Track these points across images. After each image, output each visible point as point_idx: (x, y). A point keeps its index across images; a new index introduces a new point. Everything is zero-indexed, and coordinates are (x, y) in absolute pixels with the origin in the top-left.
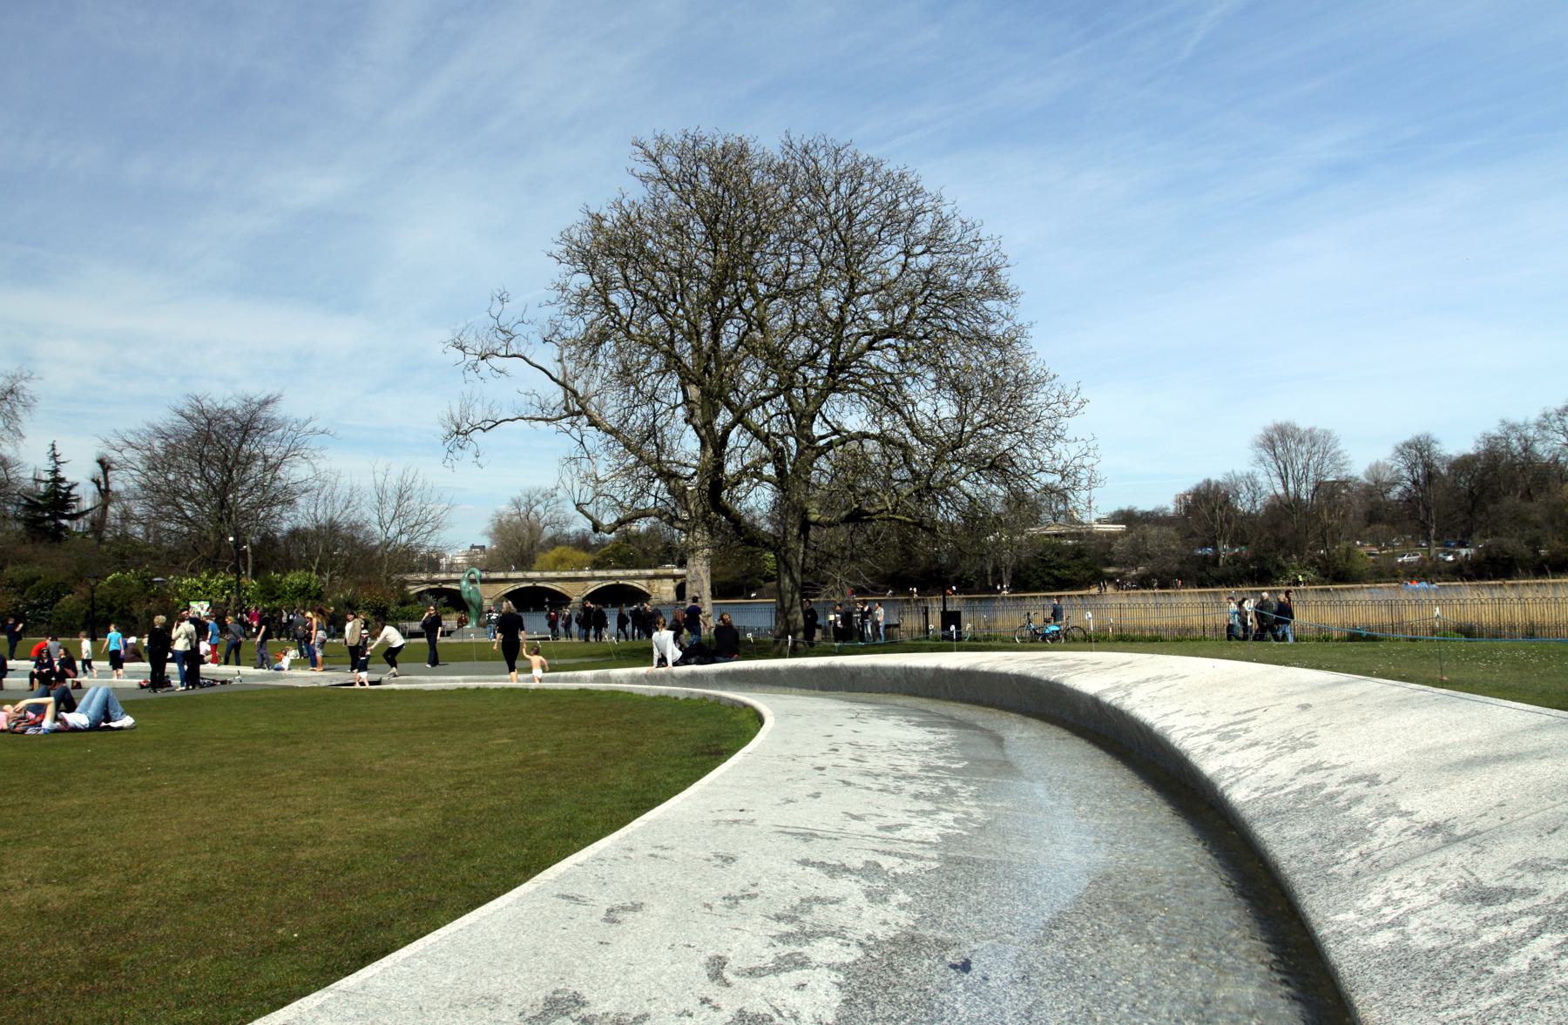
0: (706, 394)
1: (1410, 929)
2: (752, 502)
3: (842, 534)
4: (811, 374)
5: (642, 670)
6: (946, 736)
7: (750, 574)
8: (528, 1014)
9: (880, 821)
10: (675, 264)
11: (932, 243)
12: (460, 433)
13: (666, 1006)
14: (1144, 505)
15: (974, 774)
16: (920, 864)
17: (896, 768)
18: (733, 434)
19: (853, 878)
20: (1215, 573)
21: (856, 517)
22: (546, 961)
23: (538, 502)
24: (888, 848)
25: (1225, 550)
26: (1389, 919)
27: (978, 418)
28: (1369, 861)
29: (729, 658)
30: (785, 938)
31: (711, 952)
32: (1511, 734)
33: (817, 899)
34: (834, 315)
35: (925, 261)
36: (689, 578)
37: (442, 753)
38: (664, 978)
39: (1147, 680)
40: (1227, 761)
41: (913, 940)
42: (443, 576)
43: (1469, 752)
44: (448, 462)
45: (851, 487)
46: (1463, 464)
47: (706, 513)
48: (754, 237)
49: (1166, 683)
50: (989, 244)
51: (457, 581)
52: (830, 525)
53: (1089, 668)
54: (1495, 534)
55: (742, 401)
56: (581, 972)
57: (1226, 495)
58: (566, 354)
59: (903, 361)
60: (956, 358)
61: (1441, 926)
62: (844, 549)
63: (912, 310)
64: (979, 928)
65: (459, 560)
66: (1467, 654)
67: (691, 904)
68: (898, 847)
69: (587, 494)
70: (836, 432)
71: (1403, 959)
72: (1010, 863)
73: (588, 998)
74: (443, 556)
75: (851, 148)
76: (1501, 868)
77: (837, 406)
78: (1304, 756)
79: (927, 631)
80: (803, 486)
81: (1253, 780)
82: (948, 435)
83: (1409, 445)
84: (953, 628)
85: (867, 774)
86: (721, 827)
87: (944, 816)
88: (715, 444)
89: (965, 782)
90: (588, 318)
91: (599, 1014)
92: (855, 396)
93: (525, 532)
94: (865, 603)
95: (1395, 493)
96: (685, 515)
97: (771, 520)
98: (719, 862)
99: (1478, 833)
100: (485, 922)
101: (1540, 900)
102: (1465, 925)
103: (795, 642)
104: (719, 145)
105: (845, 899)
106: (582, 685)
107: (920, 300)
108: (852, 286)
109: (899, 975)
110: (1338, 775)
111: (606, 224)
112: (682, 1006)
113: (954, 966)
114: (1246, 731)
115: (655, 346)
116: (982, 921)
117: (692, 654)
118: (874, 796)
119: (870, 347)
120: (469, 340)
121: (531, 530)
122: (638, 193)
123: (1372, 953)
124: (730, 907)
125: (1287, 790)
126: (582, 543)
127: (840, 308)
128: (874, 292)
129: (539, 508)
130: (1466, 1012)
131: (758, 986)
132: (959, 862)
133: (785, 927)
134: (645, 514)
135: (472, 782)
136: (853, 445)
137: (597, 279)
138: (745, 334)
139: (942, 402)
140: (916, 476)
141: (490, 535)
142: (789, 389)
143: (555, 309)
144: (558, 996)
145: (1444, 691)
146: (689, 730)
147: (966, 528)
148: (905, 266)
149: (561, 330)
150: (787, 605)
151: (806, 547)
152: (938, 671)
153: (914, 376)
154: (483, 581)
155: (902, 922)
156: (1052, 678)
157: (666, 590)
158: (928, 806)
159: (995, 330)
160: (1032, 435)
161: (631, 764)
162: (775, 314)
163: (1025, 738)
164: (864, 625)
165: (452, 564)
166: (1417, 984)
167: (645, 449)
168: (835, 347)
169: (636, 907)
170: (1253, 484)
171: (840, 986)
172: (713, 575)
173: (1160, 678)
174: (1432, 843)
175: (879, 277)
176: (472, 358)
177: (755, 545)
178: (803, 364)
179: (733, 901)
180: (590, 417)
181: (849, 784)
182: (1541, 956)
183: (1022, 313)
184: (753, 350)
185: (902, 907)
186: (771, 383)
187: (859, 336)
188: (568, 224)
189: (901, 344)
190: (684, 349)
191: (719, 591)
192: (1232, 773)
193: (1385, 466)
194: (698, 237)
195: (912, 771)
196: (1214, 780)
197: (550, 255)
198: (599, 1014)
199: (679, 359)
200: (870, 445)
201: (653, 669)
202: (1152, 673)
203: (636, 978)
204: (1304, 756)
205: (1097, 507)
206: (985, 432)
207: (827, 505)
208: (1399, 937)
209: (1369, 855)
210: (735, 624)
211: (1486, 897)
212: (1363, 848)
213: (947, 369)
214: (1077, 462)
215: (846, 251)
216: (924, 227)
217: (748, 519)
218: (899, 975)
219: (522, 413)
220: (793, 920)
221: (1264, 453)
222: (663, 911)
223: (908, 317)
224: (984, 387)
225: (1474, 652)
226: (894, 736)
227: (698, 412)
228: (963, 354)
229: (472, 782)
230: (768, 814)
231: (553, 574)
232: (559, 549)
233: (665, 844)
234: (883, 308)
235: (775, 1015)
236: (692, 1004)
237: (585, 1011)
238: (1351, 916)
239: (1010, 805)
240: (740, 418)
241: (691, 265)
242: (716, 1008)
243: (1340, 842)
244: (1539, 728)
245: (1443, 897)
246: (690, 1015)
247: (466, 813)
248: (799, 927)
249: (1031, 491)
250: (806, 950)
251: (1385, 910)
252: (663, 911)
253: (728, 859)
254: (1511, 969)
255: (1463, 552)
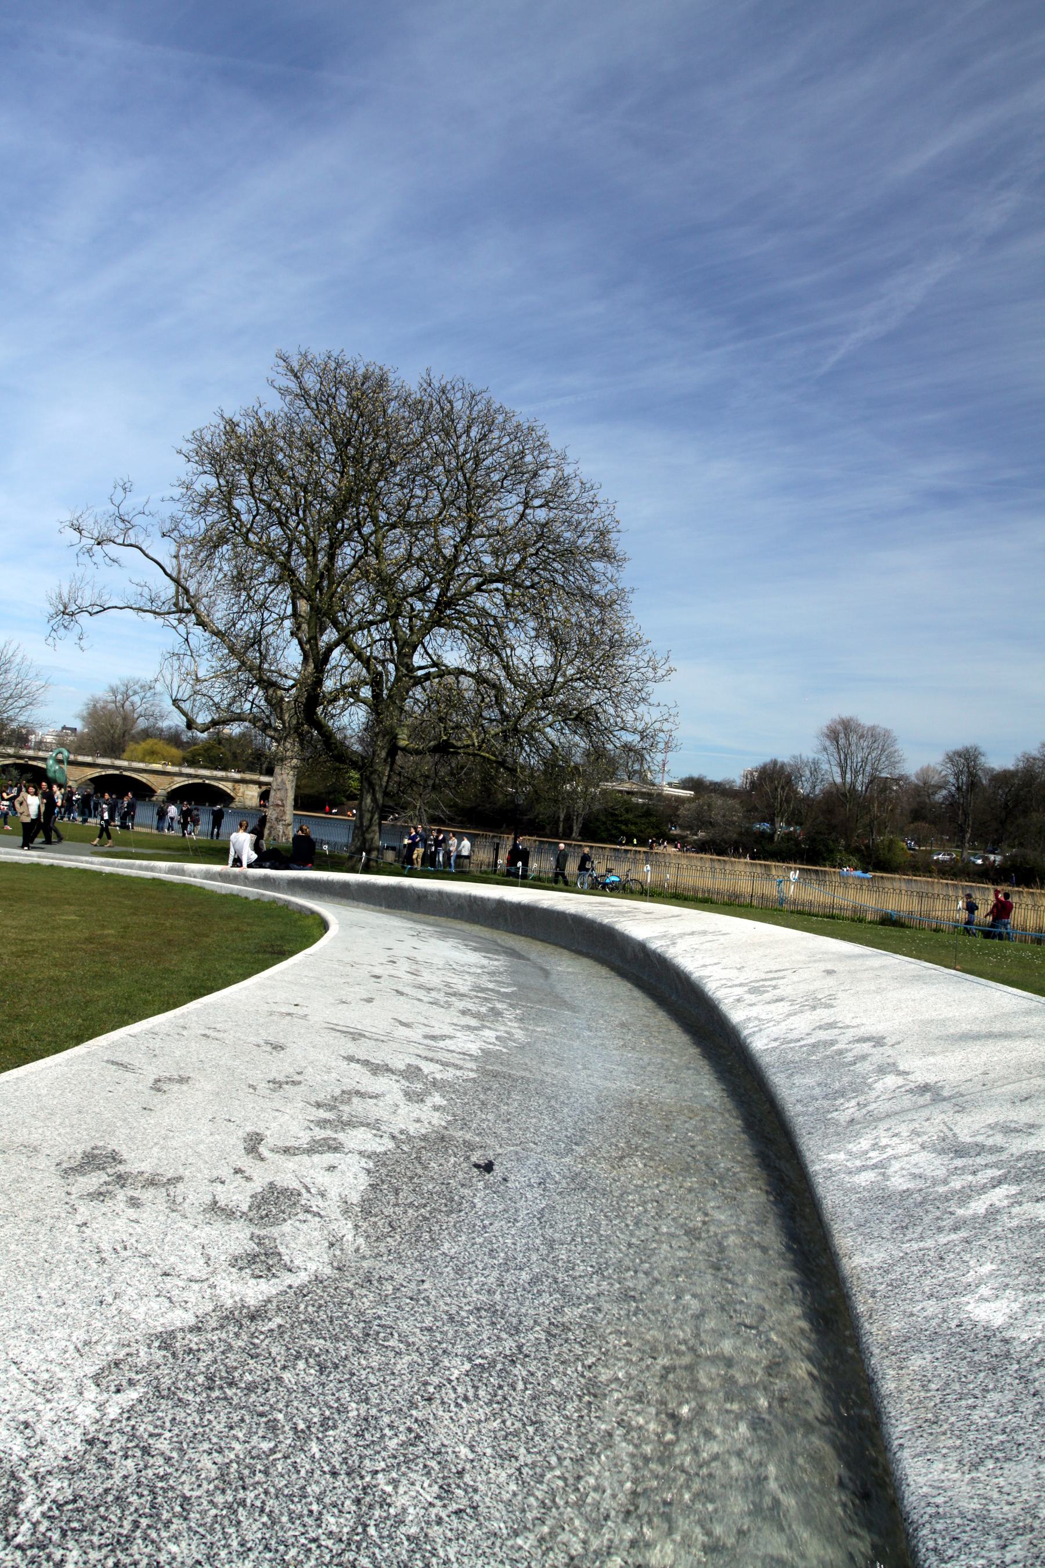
0: (315, 609)
1: (890, 1171)
2: (345, 720)
3: (427, 763)
4: (419, 605)
5: (217, 868)
6: (499, 962)
7: (333, 791)
8: (65, 1166)
9: (428, 1031)
10: (302, 480)
11: (550, 499)
12: (66, 613)
13: (200, 1171)
14: (714, 774)
15: (521, 999)
16: (459, 1073)
17: (448, 985)
18: (336, 653)
19: (394, 1077)
20: (769, 847)
21: (443, 749)
22: (88, 1120)
23: (135, 693)
24: (430, 1055)
25: (782, 827)
26: (874, 1161)
27: (570, 671)
28: (864, 1111)
29: (302, 866)
30: (322, 1123)
31: (249, 1129)
32: (1004, 1014)
33: (358, 1093)
34: (448, 552)
35: (542, 515)
36: (274, 786)
37: (8, 922)
38: (202, 1146)
39: (693, 933)
40: (753, 1012)
41: (443, 1139)
42: (31, 753)
43: (965, 1027)
44: (50, 640)
45: (441, 719)
46: (1003, 778)
47: (299, 724)
48: (382, 465)
49: (709, 937)
50: (604, 507)
51: (44, 760)
52: (417, 752)
53: (641, 916)
54: (1021, 845)
55: (350, 622)
56: (123, 1132)
57: (789, 776)
58: (183, 552)
59: (508, 605)
60: (558, 611)
61: (917, 1171)
62: (427, 777)
63: (523, 560)
64: (505, 1135)
65: (49, 739)
66: (980, 949)
67: (237, 1083)
68: (439, 1056)
69: (186, 691)
70: (435, 664)
71: (883, 1198)
72: (543, 1082)
73: (125, 1157)
74: (33, 733)
75: (485, 395)
76: (976, 1126)
77: (439, 640)
78: (823, 1015)
79: (496, 864)
80: (396, 713)
81: (775, 1031)
82: (539, 683)
83: (959, 754)
84: (520, 864)
85: (420, 987)
86: (275, 1018)
87: (487, 1033)
88: (317, 659)
89: (511, 1005)
90: (209, 520)
91: (135, 1172)
92: (458, 632)
93: (119, 720)
94: (439, 832)
95: (940, 796)
96: (278, 724)
97: (361, 740)
98: (269, 1048)
99: (962, 1095)
100: (32, 1077)
101: (1004, 1156)
102: (938, 1172)
103: (368, 860)
104: (361, 371)
105: (383, 1095)
106: (156, 875)
107: (532, 550)
108: (470, 527)
109: (425, 1168)
110: (850, 1034)
111: (240, 431)
112: (215, 1174)
113: (477, 1166)
114: (775, 987)
115: (271, 555)
116: (509, 1129)
117: (267, 857)
118: (424, 1008)
119: (479, 588)
120: (88, 523)
121: (125, 719)
122: (275, 405)
123: (854, 1190)
124: (274, 1090)
125: (802, 1043)
126: (174, 739)
127: (455, 547)
128: (490, 536)
129: (136, 699)
130: (927, 1245)
131: (291, 1164)
132: (496, 1075)
133: (323, 1114)
134: (239, 718)
135: (35, 951)
136: (450, 679)
137: (222, 482)
138: (361, 557)
139: (539, 651)
140: (505, 717)
141: (83, 719)
142: (395, 617)
143: (179, 506)
144: (96, 1152)
145: (953, 972)
146: (255, 928)
147: (545, 773)
148: (523, 516)
149: (181, 527)
150: (366, 823)
151: (391, 770)
152: (501, 903)
153: (517, 622)
154: (71, 763)
155: (435, 1122)
156: (606, 921)
157: (250, 795)
158: (474, 1022)
159: (599, 590)
160: (618, 695)
161: (195, 953)
162: (392, 543)
163: (570, 971)
164: (436, 852)
165: (41, 742)
166: (889, 1218)
167: (247, 655)
168: (446, 583)
169: (182, 1080)
170: (815, 768)
171: (369, 1171)
172: (298, 787)
173: (704, 933)
174: (921, 1101)
175: (495, 523)
176: (88, 542)
177: (343, 762)
178: (412, 595)
179: (277, 1085)
180: (198, 616)
181: (402, 994)
182: (997, 1203)
183: (627, 576)
184: (366, 574)
185: (436, 1108)
186: (379, 608)
187: (470, 576)
188: (201, 426)
189: (508, 590)
190: (300, 565)
191: (303, 802)
192: (757, 1023)
193: (934, 770)
194: (328, 457)
195: (464, 989)
196: (739, 1027)
197: (180, 452)
198: (135, 1172)
199: (292, 572)
200: (466, 682)
201: (228, 868)
202: (697, 927)
203: (175, 1143)
204: (823, 1015)
205: (670, 773)
206: (575, 684)
207: (416, 732)
208: (880, 1178)
209: (865, 1105)
210: (313, 836)
211: (960, 1151)
212: (861, 1099)
213: (548, 620)
214: (657, 725)
215: (469, 494)
216: (546, 481)
217: (339, 736)
218: (425, 1168)
219: (131, 603)
220: (332, 1108)
221: (828, 743)
222: (208, 1087)
223: (518, 566)
224: (581, 643)
225: (988, 948)
226: (451, 957)
227: (305, 626)
228: (566, 608)
229: (35, 951)
230: (322, 1010)
231: (141, 765)
232: (150, 742)
233: (218, 1026)
234: (495, 553)
235: (303, 1191)
236: (226, 1172)
237: (121, 1168)
238: (842, 1156)
239: (550, 1031)
240: (344, 639)
241: (317, 483)
242: (248, 1179)
243: (842, 1093)
244: (1028, 1012)
245: (923, 1147)
246: (223, 1183)
247: (25, 980)
248: (337, 1113)
249: (610, 746)
250: (341, 1136)
251: (871, 1154)
252: (208, 1087)
253: (278, 1047)
254: (971, 1212)
255: (992, 857)
